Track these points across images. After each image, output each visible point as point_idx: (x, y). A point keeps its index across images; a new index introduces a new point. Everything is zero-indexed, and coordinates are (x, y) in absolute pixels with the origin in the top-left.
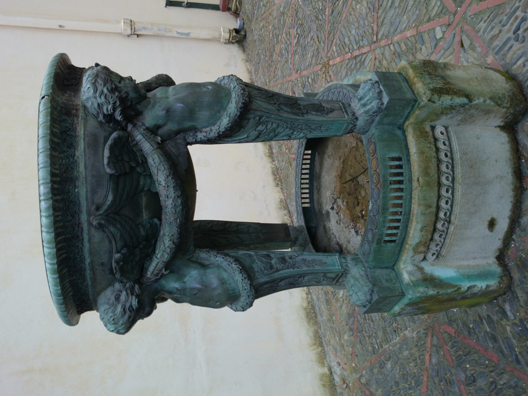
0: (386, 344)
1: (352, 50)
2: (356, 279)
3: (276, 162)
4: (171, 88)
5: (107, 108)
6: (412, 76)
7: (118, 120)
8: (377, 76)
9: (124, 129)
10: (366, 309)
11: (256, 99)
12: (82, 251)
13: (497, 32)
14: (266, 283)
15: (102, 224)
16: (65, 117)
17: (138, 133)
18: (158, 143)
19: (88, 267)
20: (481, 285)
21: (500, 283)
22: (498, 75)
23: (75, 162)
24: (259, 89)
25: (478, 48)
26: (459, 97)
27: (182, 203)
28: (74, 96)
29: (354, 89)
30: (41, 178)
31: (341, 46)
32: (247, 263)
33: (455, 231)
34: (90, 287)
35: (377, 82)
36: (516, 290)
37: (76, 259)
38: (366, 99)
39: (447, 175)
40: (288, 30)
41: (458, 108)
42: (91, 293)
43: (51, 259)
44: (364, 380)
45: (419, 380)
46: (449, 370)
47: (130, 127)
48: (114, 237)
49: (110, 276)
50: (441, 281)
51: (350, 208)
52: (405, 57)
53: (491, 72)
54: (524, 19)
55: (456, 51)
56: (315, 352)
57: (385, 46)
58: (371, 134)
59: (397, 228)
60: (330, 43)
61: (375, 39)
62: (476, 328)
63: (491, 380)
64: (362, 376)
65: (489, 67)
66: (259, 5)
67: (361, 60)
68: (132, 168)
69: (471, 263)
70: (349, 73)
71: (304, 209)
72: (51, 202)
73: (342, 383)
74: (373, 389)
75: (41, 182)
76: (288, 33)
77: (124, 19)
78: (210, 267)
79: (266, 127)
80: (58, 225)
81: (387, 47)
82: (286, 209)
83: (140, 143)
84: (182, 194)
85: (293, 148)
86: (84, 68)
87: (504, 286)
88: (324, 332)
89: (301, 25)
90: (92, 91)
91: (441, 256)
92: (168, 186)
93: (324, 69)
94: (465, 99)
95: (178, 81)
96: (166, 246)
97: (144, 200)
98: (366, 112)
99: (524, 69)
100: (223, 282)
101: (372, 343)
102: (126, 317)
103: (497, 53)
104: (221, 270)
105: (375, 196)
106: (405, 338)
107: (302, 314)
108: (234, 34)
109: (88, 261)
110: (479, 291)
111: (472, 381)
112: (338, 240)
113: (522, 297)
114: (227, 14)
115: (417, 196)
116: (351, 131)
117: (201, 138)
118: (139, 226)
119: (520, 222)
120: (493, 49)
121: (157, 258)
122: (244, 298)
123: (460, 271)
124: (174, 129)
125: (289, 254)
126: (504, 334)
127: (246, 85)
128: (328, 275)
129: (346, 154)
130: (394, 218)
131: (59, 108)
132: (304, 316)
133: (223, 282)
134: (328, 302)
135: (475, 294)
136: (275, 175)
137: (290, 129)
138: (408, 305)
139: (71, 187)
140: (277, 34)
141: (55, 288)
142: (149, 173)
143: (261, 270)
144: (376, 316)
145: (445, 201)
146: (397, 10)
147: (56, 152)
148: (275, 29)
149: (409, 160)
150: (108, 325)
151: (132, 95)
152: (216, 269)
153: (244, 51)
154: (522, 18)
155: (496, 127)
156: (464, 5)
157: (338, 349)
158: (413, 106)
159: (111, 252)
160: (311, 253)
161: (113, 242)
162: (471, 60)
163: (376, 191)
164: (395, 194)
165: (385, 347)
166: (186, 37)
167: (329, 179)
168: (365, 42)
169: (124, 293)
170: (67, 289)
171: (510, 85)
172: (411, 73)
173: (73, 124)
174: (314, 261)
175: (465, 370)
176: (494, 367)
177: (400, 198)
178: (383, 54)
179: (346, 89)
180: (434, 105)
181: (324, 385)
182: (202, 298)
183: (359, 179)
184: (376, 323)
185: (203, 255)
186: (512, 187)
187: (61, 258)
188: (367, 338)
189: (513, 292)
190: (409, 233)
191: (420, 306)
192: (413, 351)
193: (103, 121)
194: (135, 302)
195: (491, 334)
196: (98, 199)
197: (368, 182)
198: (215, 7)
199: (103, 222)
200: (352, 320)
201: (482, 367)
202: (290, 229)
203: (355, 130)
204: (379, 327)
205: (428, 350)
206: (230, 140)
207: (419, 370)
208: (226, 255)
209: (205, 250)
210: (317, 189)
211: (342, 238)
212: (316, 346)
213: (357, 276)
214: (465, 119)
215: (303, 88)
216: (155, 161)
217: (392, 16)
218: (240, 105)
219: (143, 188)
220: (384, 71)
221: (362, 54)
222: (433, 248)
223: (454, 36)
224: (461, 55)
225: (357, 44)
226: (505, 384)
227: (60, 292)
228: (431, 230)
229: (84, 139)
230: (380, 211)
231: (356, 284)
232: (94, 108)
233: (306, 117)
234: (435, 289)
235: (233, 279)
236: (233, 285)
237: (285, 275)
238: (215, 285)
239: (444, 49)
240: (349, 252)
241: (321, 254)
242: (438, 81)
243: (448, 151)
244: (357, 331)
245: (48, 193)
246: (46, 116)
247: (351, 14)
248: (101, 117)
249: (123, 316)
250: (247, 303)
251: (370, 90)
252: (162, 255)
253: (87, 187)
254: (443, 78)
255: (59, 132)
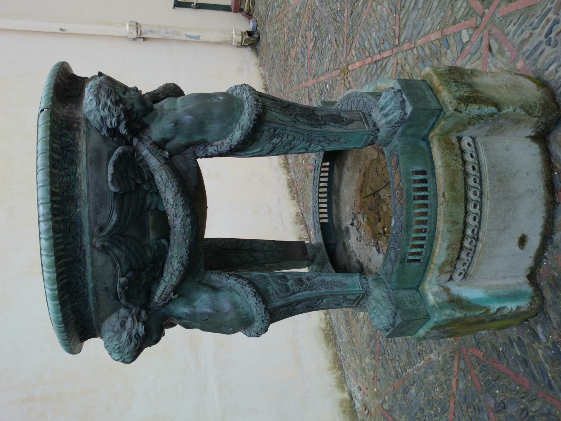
0: (410, 368)
1: (373, 54)
2: (378, 301)
3: (292, 173)
4: (179, 99)
5: (111, 122)
6: (437, 84)
7: (122, 134)
8: (400, 83)
9: (129, 144)
10: (388, 333)
11: (271, 110)
12: (85, 276)
13: (528, 35)
14: (282, 306)
15: (106, 246)
16: (66, 132)
17: (144, 148)
18: (166, 158)
19: (90, 292)
20: (511, 306)
21: (531, 304)
22: (529, 82)
23: (77, 180)
24: (274, 99)
25: (507, 53)
26: (487, 106)
27: (191, 223)
28: (76, 108)
29: (375, 98)
30: (40, 197)
31: (361, 50)
32: (262, 285)
33: (483, 249)
34: (93, 314)
35: (399, 91)
36: (549, 311)
37: (78, 283)
38: (388, 109)
39: (474, 190)
40: (304, 32)
41: (486, 118)
42: (94, 319)
43: (51, 284)
44: (387, 406)
45: (445, 407)
46: (478, 396)
47: (135, 141)
48: (118, 260)
49: (115, 301)
50: (469, 302)
51: (372, 224)
52: (428, 63)
53: (521, 79)
54: (556, 22)
55: (483, 56)
56: (334, 376)
57: (408, 50)
58: (393, 146)
59: (421, 246)
60: (349, 46)
61: (397, 43)
62: (506, 351)
63: (522, 406)
64: (384, 401)
65: (519, 73)
66: (273, 6)
67: (382, 65)
68: (138, 186)
69: (501, 282)
70: (370, 78)
71: (322, 224)
72: (51, 223)
73: (364, 409)
74: (396, 416)
75: (40, 202)
76: (304, 36)
77: (130, 22)
78: (222, 291)
79: (282, 139)
80: (58, 248)
81: (410, 51)
82: (302, 224)
83: (146, 159)
84: (191, 212)
85: (309, 161)
86: (87, 78)
87: (536, 306)
88: (344, 355)
89: (318, 27)
90: (95, 103)
91: (468, 275)
92: (176, 205)
93: (342, 75)
94: (494, 108)
95: (187, 91)
96: (175, 268)
97: (151, 220)
98: (388, 123)
99: (558, 75)
100: (235, 306)
101: (395, 367)
102: (132, 345)
103: (527, 58)
104: (234, 293)
105: (398, 213)
106: (430, 362)
107: (321, 336)
108: (247, 37)
109: (91, 285)
110: (509, 312)
111: (501, 407)
112: (359, 258)
113: (554, 318)
114: (239, 15)
115: (442, 213)
116: (372, 143)
117: (211, 152)
118: (146, 248)
119: (552, 239)
120: (523, 54)
121: (164, 281)
122: (259, 323)
123: (489, 292)
124: (183, 143)
125: (307, 275)
126: (535, 358)
127: (260, 95)
128: (348, 297)
129: (367, 167)
130: (418, 236)
131: (59, 122)
132: (322, 338)
133: (235, 306)
134: (348, 322)
135: (505, 316)
136: (291, 188)
137: (307, 141)
138: (434, 328)
139: (72, 207)
140: (293, 37)
141: (56, 315)
142: (156, 191)
143: (277, 293)
144: (399, 339)
145: (472, 217)
146: (420, 12)
147: (56, 169)
148: (291, 31)
149: (434, 174)
150: (113, 354)
151: (138, 107)
152: (228, 292)
153: (257, 54)
154: (554, 21)
155: (526, 137)
156: (493, 7)
157: (359, 372)
158: (438, 116)
159: (115, 277)
160: (330, 274)
161: (118, 265)
162: (500, 65)
163: (399, 206)
164: (420, 210)
165: (409, 371)
166: (195, 40)
167: (349, 193)
168: (387, 46)
169: (130, 319)
170: (69, 316)
171: (542, 93)
172: (436, 80)
173: (74, 138)
174: (333, 282)
175: (494, 396)
176: (525, 392)
177: (425, 214)
178: (405, 59)
179: (366, 98)
180: (461, 115)
181: (344, 412)
182: (213, 323)
183: (380, 194)
184: (399, 346)
185: (215, 277)
186: (544, 201)
187: (61, 283)
188: (390, 362)
189: (546, 314)
190: (435, 251)
191: (446, 329)
192: (438, 376)
193: (107, 135)
194: (141, 329)
195: (522, 358)
196: (102, 220)
197: (390, 196)
198: (226, 8)
199: (107, 244)
200: (373, 342)
201: (513, 392)
202: (307, 247)
203: (376, 142)
204: (402, 349)
205: (455, 374)
206: (242, 154)
207: (446, 396)
208: (239, 277)
209: (216, 271)
210: (335, 203)
211: (363, 256)
212: (336, 370)
213: (379, 298)
214: (493, 129)
215: (321, 95)
216: (162, 178)
217: (416, 18)
218: (254, 116)
219: (150, 206)
220: (407, 77)
221: (384, 59)
222: (460, 267)
223: (482, 40)
224: (489, 60)
225: (378, 48)
226: (537, 411)
227: (61, 319)
228: (458, 248)
229: (86, 155)
230: (404, 228)
231: (378, 306)
232: (97, 121)
233: (324, 128)
234: (462, 311)
235: (247, 303)
236: (247, 309)
237: (302, 297)
238: (227, 310)
239: (470, 53)
240: (370, 272)
241: (341, 274)
242: (465, 89)
243: (475, 163)
244: (378, 354)
245: (47, 214)
246: (46, 130)
247: (371, 16)
248: (104, 131)
249: (128, 345)
250: (262, 329)
251: (392, 99)
252: (171, 279)
253: (89, 207)
254: (470, 85)
255: (59, 147)
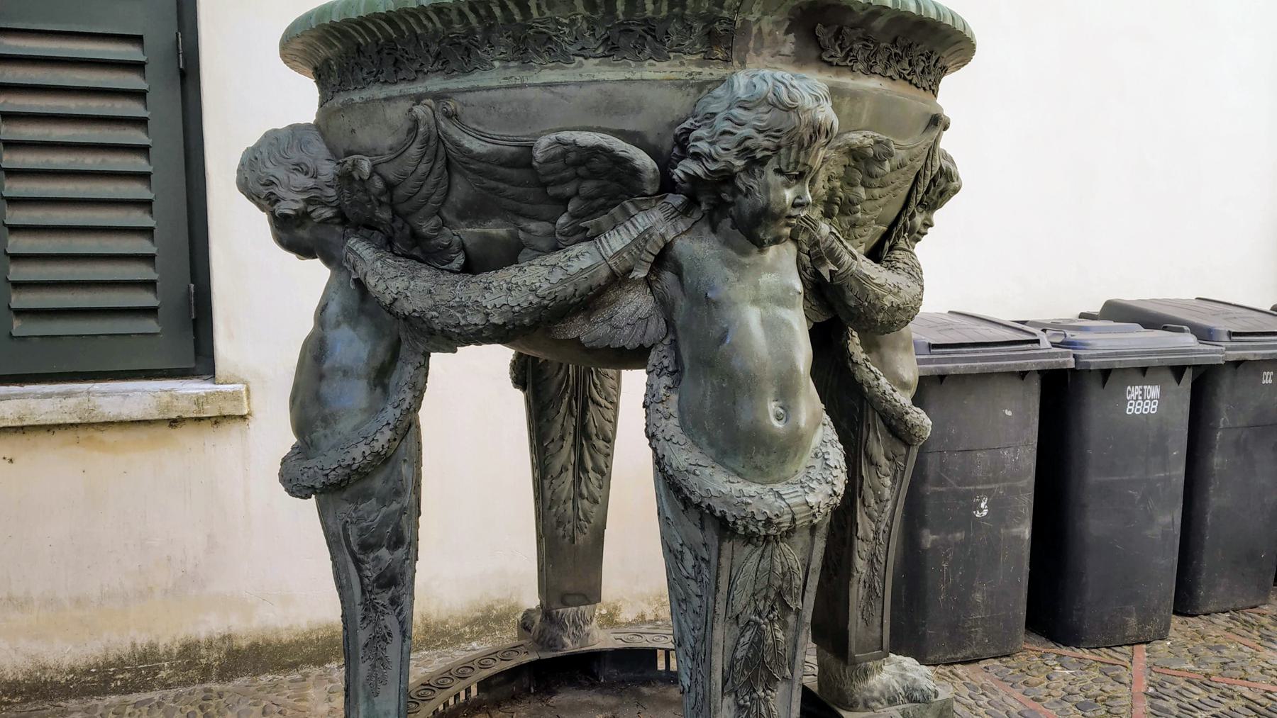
11: (762, 557)
16: (698, 27)
83: (628, 224)
97: (498, 230)
118: (437, 217)
139: (502, 50)
199: (421, 130)
229: (628, 81)
